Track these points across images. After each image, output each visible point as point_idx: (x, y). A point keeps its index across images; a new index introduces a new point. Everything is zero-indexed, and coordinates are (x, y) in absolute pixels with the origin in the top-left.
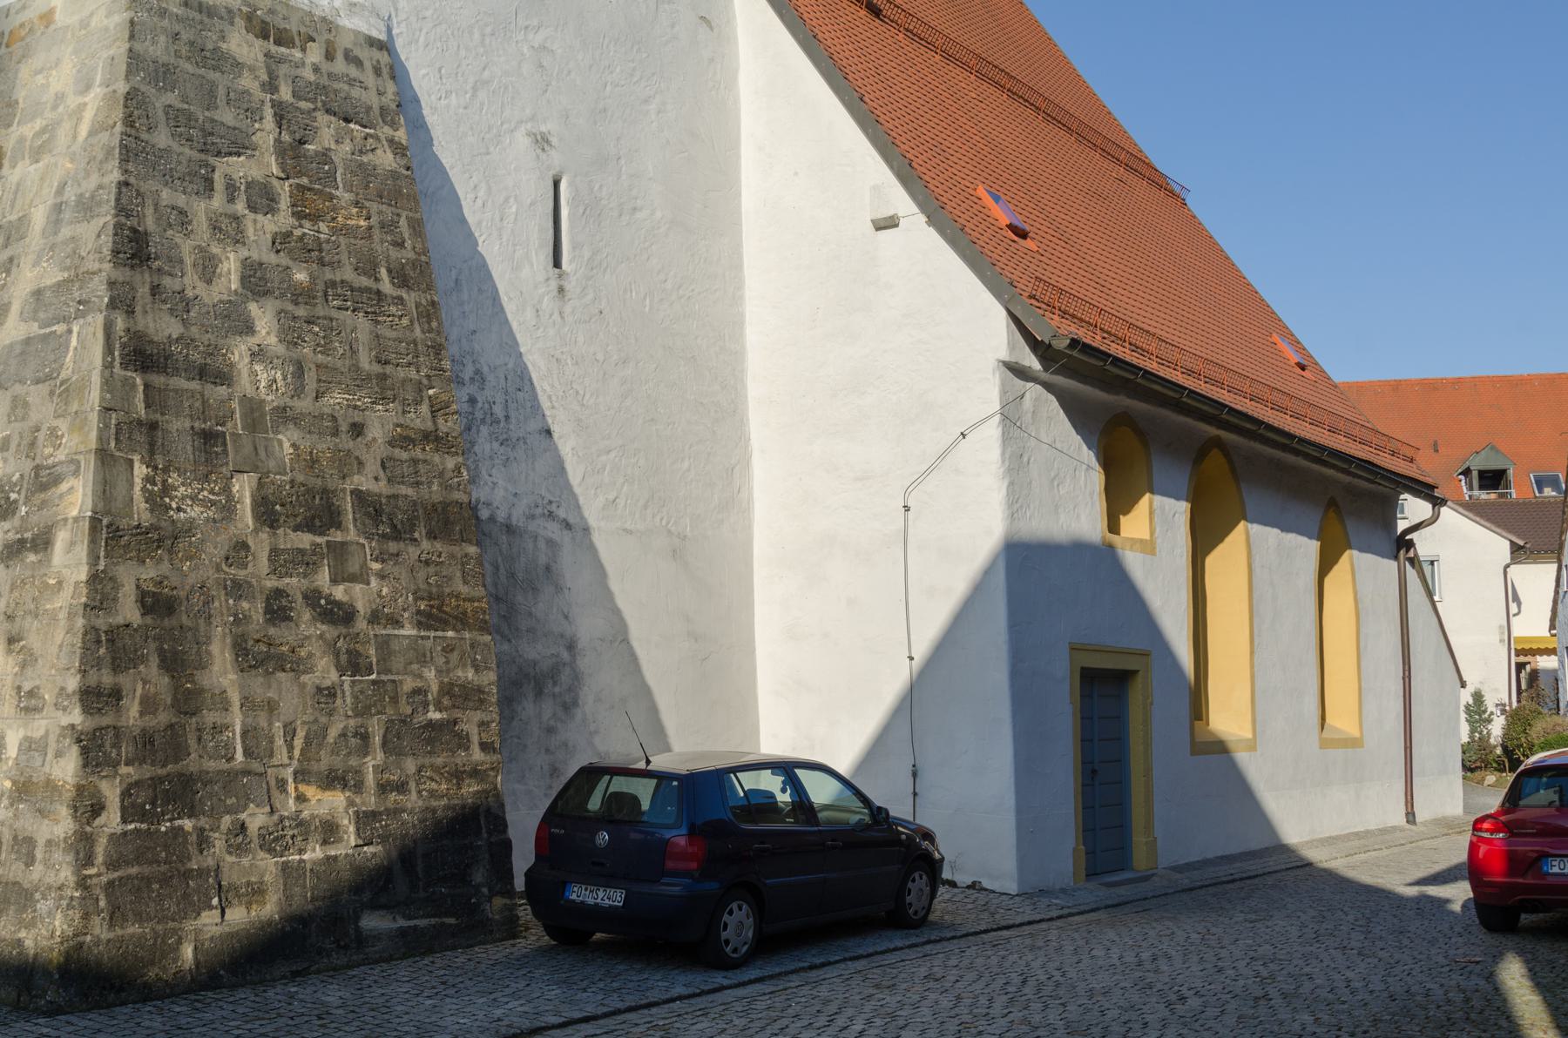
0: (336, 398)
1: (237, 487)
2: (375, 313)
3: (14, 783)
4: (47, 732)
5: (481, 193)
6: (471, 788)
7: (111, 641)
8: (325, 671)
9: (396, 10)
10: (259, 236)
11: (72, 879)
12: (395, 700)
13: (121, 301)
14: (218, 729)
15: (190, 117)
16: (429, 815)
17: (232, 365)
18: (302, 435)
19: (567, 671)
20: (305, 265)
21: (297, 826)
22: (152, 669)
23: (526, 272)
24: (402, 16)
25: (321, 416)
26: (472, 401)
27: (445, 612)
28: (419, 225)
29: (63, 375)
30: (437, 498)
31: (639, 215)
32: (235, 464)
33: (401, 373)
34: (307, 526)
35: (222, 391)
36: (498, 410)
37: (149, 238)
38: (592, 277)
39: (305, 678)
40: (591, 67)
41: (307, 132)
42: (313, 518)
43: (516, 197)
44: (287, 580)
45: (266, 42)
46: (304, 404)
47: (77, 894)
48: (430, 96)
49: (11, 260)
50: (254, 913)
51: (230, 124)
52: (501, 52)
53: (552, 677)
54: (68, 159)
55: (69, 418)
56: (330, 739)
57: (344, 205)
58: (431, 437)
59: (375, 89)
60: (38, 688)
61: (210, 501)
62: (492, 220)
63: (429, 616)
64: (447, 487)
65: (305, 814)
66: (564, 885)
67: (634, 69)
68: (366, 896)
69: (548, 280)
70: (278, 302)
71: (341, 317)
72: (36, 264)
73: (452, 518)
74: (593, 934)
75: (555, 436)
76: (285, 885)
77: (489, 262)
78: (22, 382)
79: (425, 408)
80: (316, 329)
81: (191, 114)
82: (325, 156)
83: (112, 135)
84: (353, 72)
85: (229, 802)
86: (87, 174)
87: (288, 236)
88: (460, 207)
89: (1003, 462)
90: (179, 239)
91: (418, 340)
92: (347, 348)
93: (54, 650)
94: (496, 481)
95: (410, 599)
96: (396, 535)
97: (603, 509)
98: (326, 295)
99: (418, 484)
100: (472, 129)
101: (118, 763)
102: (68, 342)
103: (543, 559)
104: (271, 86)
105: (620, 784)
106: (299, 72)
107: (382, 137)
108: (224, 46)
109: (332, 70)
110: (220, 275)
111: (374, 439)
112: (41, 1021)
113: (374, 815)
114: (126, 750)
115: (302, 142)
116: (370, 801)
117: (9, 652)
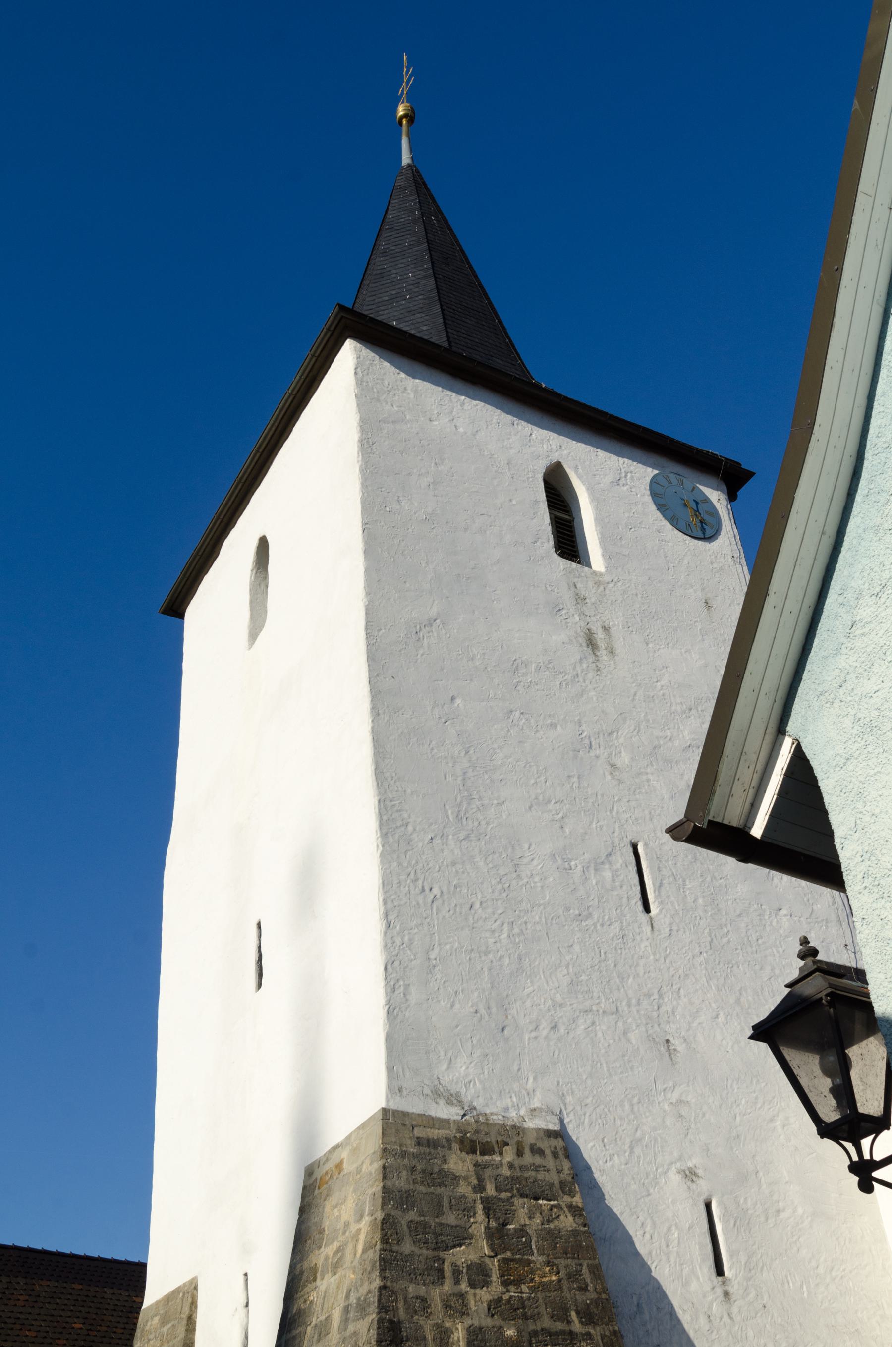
5: (648, 1228)
10: (478, 1306)
15: (425, 1226)
20: (513, 1322)
23: (694, 1286)
24: (570, 1108)
28: (598, 1271)
37: (401, 1325)
38: (752, 1277)
41: (508, 1216)
43: (676, 1224)
45: (475, 1155)
48: (598, 1162)
52: (647, 1114)
54: (352, 1271)
57: (539, 1266)
59: (555, 1169)
62: (660, 1247)
67: (756, 1098)
69: (713, 1288)
77: (662, 1283)
81: (426, 1223)
82: (522, 1231)
83: (375, 1252)
84: (538, 1160)
87: (500, 1302)
100: (633, 1179)
104: (480, 1188)
106: (499, 1171)
107: (563, 1205)
108: (446, 1167)
109: (522, 1163)
115: (505, 1224)
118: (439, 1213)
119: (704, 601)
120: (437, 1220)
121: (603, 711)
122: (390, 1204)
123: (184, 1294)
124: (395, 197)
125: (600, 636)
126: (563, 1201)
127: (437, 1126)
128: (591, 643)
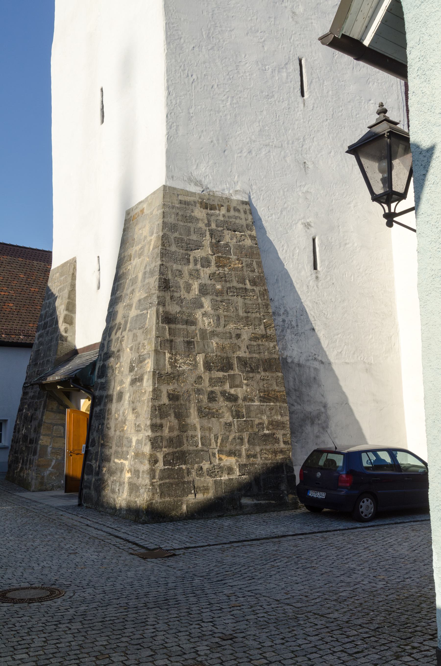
0: (231, 326)
1: (198, 358)
2: (244, 296)
3: (135, 453)
4: (142, 438)
5: (285, 248)
6: (280, 457)
7: (160, 409)
8: (228, 417)
9: (252, 189)
11: (149, 483)
12: (252, 427)
13: (161, 303)
14: (193, 437)
15: (182, 240)
16: (265, 466)
17: (196, 319)
18: (219, 339)
19: (324, 415)
21: (219, 468)
22: (172, 418)
23: (303, 273)
24: (254, 191)
25: (226, 333)
26: (284, 321)
27: (270, 396)
29: (146, 327)
30: (267, 357)
31: (348, 246)
32: (197, 351)
33: (254, 315)
34: (221, 369)
35: (193, 327)
36: (294, 323)
39: (221, 420)
40: (326, 195)
42: (224, 367)
43: (298, 247)
44: (215, 388)
46: (220, 329)
47: (151, 488)
49: (133, 290)
50: (205, 496)
51: (195, 240)
52: (291, 197)
53: (318, 418)
55: (147, 340)
56: (230, 440)
58: (265, 337)
60: (140, 424)
61: (190, 363)
63: (264, 398)
64: (270, 353)
65: (222, 464)
66: (307, 490)
67: (344, 193)
68: (243, 492)
70: (211, 297)
71: (233, 299)
72: (139, 291)
73: (272, 364)
74: (323, 509)
75: (316, 330)
76: (215, 487)
77: (289, 271)
78: (136, 329)
79: (262, 327)
80: (224, 304)
83: (158, 249)
84: (237, 214)
85: (197, 460)
86: (152, 263)
88: (277, 253)
89: (109, 409)
90: (179, 280)
91: (260, 303)
92: (235, 309)
93: (144, 412)
94: (293, 348)
95: (257, 392)
96: (252, 371)
97: (336, 355)
98: (227, 292)
99: (260, 353)
100: (281, 225)
101: (162, 447)
102: (147, 316)
103: (312, 375)
104: (209, 225)
105: (331, 456)
106: (218, 218)
108: (193, 214)
109: (229, 215)
110: (192, 290)
111: (244, 339)
112: (140, 525)
113: (245, 465)
114: (165, 443)
116: (244, 460)
117: (133, 413)
120: (188, 237)
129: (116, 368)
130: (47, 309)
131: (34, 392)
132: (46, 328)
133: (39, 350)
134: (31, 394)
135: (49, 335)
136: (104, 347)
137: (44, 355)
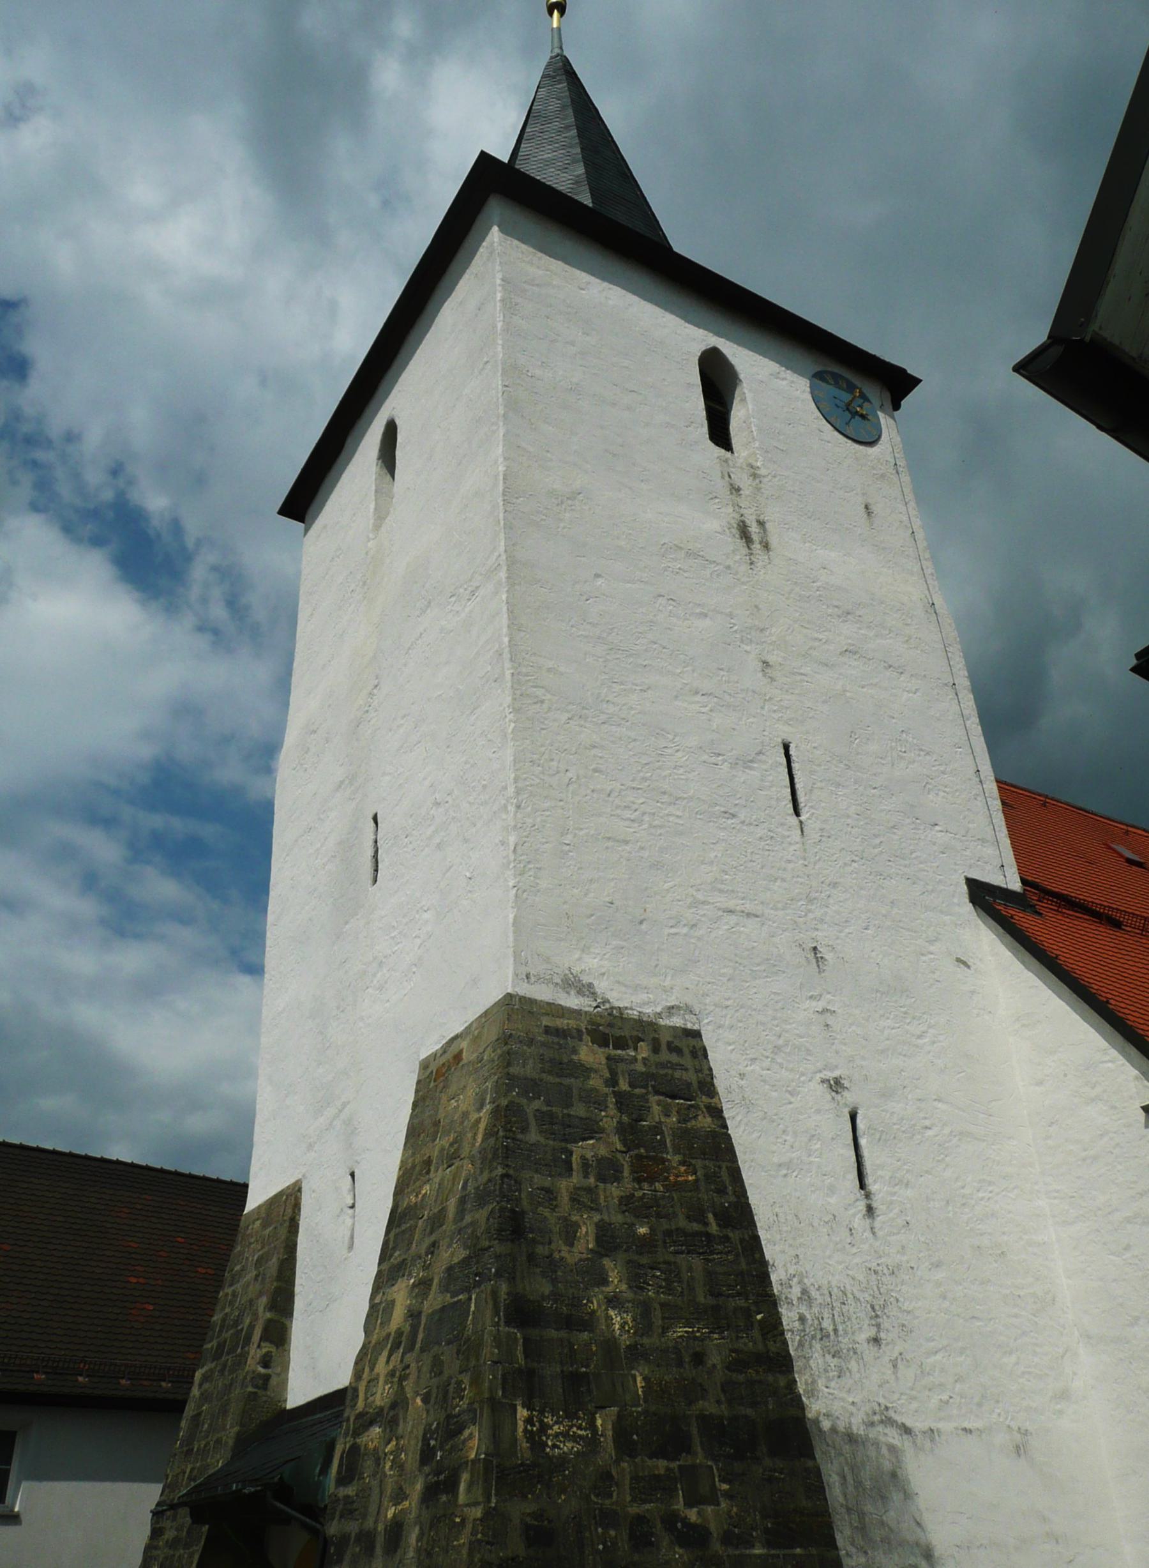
15: (551, 1115)
35: (585, 1336)
36: (827, 1324)
45: (607, 1049)
55: (469, 1374)
72: (449, 1246)
79: (756, 1333)
82: (657, 1129)
84: (674, 1058)
86: (482, 1172)
104: (613, 1082)
106: (632, 1067)
108: (575, 1057)
118: (569, 1105)
119: (863, 506)
120: (565, 1111)
121: (756, 607)
122: (515, 1091)
123: (287, 1196)
124: (529, 130)
125: (754, 529)
126: (702, 1102)
127: (567, 1015)
128: (744, 533)
129: (386, 1454)
130: (227, 1310)
131: (177, 1530)
132: (220, 1358)
133: (199, 1414)
134: (169, 1535)
135: (226, 1373)
136: (358, 1396)
137: (210, 1425)
